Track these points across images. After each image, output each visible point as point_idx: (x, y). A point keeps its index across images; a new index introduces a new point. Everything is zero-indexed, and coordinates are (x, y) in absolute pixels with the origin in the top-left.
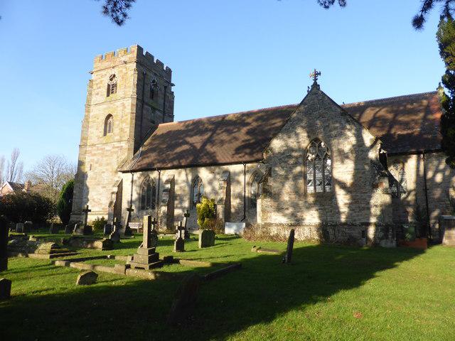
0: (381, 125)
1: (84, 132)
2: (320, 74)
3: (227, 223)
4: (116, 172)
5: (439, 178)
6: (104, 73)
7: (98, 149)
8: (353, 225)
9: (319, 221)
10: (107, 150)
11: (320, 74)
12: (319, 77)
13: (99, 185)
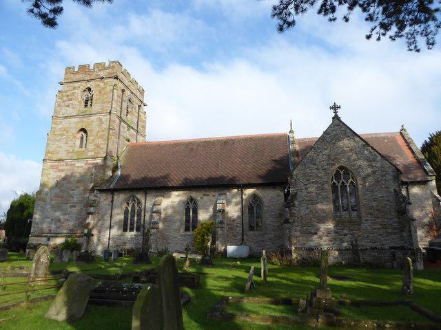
0: (244, 251)
1: (50, 145)
2: (340, 107)
3: (404, 159)
4: (92, 190)
5: (366, 152)
6: (76, 85)
7: (66, 165)
8: (382, 249)
9: (328, 283)
10: (78, 167)
11: (340, 107)
12: (339, 110)
13: (67, 203)
